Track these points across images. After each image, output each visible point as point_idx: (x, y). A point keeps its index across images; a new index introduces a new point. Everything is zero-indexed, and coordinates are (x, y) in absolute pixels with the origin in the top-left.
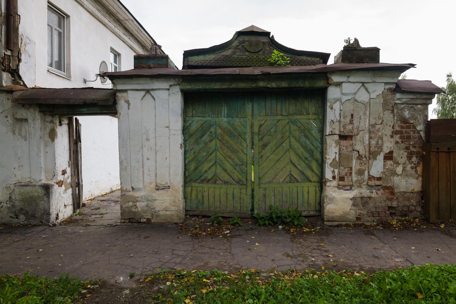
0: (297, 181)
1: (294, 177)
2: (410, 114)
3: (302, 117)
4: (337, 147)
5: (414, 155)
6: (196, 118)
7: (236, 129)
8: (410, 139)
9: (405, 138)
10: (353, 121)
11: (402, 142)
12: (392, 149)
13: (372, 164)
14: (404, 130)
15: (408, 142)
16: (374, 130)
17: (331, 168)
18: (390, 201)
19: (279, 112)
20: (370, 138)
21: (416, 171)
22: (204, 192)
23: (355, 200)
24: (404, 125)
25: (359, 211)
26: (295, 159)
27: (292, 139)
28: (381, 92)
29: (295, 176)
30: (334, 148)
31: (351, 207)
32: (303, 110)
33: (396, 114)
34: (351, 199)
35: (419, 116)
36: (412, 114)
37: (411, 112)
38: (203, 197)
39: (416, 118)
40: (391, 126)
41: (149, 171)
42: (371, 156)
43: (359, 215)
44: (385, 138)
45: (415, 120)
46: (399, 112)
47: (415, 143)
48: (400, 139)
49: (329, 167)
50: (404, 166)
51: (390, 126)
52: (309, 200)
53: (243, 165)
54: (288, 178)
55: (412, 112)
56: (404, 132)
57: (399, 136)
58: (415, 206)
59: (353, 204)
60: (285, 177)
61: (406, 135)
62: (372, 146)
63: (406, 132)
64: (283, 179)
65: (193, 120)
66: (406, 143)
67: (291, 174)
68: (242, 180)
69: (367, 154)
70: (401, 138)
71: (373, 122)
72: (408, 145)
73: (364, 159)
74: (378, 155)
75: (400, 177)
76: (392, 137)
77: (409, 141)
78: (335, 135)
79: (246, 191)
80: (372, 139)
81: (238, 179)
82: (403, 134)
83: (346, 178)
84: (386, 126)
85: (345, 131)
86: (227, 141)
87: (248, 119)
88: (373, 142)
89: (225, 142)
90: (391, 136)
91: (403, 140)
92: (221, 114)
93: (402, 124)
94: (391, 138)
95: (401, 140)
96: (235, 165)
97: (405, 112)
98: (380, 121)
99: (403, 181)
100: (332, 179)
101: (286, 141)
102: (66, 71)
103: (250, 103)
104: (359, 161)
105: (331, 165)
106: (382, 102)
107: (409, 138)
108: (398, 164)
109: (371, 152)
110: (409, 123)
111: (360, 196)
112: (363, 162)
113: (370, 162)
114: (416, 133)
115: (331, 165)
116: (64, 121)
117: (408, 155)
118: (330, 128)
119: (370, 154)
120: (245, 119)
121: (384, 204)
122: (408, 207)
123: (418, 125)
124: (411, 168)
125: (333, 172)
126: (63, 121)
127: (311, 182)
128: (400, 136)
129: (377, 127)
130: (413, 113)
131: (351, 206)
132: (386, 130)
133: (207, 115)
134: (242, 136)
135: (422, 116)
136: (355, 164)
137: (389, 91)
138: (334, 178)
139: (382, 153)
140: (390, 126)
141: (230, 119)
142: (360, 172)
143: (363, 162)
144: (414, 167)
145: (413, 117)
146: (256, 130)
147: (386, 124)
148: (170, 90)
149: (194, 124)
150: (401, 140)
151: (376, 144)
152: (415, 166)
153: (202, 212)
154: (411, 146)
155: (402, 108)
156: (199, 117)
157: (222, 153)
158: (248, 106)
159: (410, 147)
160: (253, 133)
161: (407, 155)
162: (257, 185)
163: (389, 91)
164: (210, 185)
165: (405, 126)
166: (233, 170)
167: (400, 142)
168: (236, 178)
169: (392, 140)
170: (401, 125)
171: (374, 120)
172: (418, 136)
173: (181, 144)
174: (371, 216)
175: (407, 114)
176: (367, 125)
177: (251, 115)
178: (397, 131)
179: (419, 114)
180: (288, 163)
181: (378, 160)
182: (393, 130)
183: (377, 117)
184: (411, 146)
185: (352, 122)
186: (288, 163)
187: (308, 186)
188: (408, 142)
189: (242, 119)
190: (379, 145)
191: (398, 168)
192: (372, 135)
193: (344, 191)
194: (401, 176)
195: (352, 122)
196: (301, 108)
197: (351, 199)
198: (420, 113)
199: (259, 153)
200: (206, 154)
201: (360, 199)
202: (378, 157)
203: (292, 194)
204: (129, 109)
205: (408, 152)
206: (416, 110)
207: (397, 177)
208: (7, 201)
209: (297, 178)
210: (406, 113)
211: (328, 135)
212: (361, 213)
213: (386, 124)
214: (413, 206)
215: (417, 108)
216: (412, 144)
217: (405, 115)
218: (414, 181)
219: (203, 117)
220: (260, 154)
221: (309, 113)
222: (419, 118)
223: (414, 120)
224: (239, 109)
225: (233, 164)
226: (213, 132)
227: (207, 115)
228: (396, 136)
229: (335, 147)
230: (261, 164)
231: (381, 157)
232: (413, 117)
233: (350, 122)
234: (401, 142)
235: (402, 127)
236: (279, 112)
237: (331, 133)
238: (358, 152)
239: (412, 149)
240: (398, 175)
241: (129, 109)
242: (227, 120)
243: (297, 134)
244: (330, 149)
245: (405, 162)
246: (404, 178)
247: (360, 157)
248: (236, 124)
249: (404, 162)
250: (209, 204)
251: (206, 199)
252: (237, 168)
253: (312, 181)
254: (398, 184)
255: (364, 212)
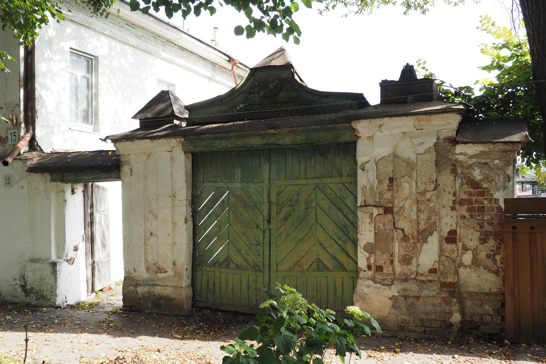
0: (327, 269)
1: (323, 263)
2: (483, 173)
3: (333, 180)
4: (372, 223)
5: (490, 237)
6: (207, 183)
7: (251, 197)
8: (484, 212)
9: (475, 211)
10: (392, 186)
11: (472, 216)
12: (454, 228)
13: (421, 250)
14: (474, 198)
15: (481, 216)
16: (424, 199)
17: (364, 252)
18: (448, 304)
19: (302, 174)
20: (419, 210)
21: (495, 261)
22: (216, 278)
23: (396, 299)
24: (473, 191)
25: (402, 317)
26: (324, 240)
27: (320, 212)
28: (432, 145)
29: (325, 262)
30: (368, 224)
31: (389, 309)
32: (334, 171)
33: (461, 174)
34: (390, 299)
35: (496, 176)
36: (485, 174)
37: (484, 171)
38: (214, 284)
39: (492, 180)
40: (452, 193)
41: (152, 250)
42: (420, 236)
43: (402, 322)
44: (443, 212)
45: (491, 184)
46: (465, 171)
47: (492, 219)
48: (468, 211)
49: (362, 251)
50: (475, 253)
51: (450, 193)
52: (344, 297)
53: (259, 244)
54: (315, 264)
55: (485, 172)
56: (474, 201)
57: (466, 207)
58: (491, 316)
59: (392, 306)
60: (311, 262)
61: (478, 205)
62: (420, 222)
63: (477, 202)
64: (308, 266)
65: (204, 186)
66: (477, 218)
67: (319, 259)
68: (258, 264)
69: (415, 234)
70: (469, 210)
71: (422, 188)
72: (481, 222)
73: (412, 241)
74: (430, 236)
75: (468, 269)
76: (453, 208)
77: (482, 215)
78: (370, 206)
79: (263, 280)
80: (421, 212)
81: (253, 263)
82: (472, 204)
83: (384, 268)
84: (443, 193)
85: (382, 201)
86: (241, 213)
87: (264, 184)
88: (423, 216)
89: (239, 214)
90: (451, 207)
91: (473, 213)
92: (234, 179)
93: (470, 190)
94: (452, 210)
95: (469, 214)
96: (250, 245)
97: (475, 170)
98: (433, 186)
99: (473, 274)
100: (366, 269)
101: (318, 213)
102: (94, 123)
103: (267, 164)
104: (404, 244)
105: (365, 248)
106: (434, 158)
107: (482, 210)
108: (465, 249)
109: (420, 231)
110: (481, 188)
111: (404, 294)
112: (411, 245)
113: (419, 245)
114: (493, 203)
115: (365, 248)
116: (77, 189)
117: (482, 237)
118: (362, 197)
119: (419, 235)
120: (261, 184)
121: (438, 309)
122: (481, 316)
123: (496, 190)
124: (487, 257)
125: (368, 259)
126: (76, 188)
127: (347, 271)
128: (468, 207)
129: (428, 195)
130: (487, 173)
131: (390, 309)
132: (443, 198)
133: (219, 180)
134: (258, 207)
135: (501, 176)
136: (397, 248)
137: (446, 141)
138: (369, 267)
139: (435, 234)
140: (450, 193)
141: (245, 184)
142: (406, 260)
143: (411, 245)
144: (492, 255)
145: (487, 178)
146: (274, 198)
147: (444, 190)
148: (173, 151)
149: (205, 192)
150: (469, 214)
151: (427, 220)
152: (492, 253)
153: (213, 304)
154: (486, 223)
155: (469, 166)
156: (211, 182)
157: (236, 229)
158: (264, 167)
159: (483, 224)
160: (270, 202)
161: (480, 235)
162: (274, 273)
163: (446, 141)
164: (223, 270)
165: (475, 192)
166: (248, 250)
167: (468, 216)
168: (251, 262)
169: (454, 213)
170: (469, 192)
171: (423, 184)
172: (496, 207)
173: (186, 218)
174: (419, 325)
175: (477, 174)
176: (414, 191)
177: (268, 178)
178: (462, 199)
179: (497, 174)
180: (315, 244)
181: (430, 243)
182: (454, 198)
183: (427, 181)
184: (486, 223)
185: (391, 188)
186: (315, 244)
187: (342, 276)
188: (481, 216)
189: (258, 184)
190: (431, 221)
191: (464, 255)
192: (422, 207)
193: (382, 286)
194: (471, 268)
195: (391, 188)
196: (331, 169)
197: (390, 299)
198: (499, 172)
199: (277, 230)
200: (218, 229)
201: (402, 299)
202: (430, 239)
203: (320, 288)
204: (131, 176)
205: (481, 232)
206: (491, 168)
207: (464, 269)
208: (20, 278)
209: (328, 264)
210: (475, 172)
211: (360, 206)
212: (404, 320)
213: (444, 190)
214: (489, 315)
215: (494, 165)
216: (487, 220)
217: (474, 175)
218: (492, 277)
219: (215, 182)
220: (278, 231)
221: (343, 175)
222: (496, 180)
223: (489, 184)
224: (254, 171)
225: (247, 243)
226: (226, 201)
227: (219, 180)
228: (461, 207)
229: (369, 223)
230: (280, 245)
231: (434, 241)
232: (487, 178)
233: (389, 188)
234: (469, 217)
235: (470, 194)
236: (302, 174)
237: (363, 204)
238: (403, 230)
239: (487, 227)
240: (466, 267)
241: (131, 176)
242: (241, 186)
243: (325, 204)
244: (363, 226)
245: (477, 247)
246: (475, 271)
247: (405, 238)
248: (251, 190)
249: (475, 247)
250: (221, 295)
251: (217, 287)
252: (253, 248)
253: (348, 270)
254: (466, 280)
255: (410, 319)
